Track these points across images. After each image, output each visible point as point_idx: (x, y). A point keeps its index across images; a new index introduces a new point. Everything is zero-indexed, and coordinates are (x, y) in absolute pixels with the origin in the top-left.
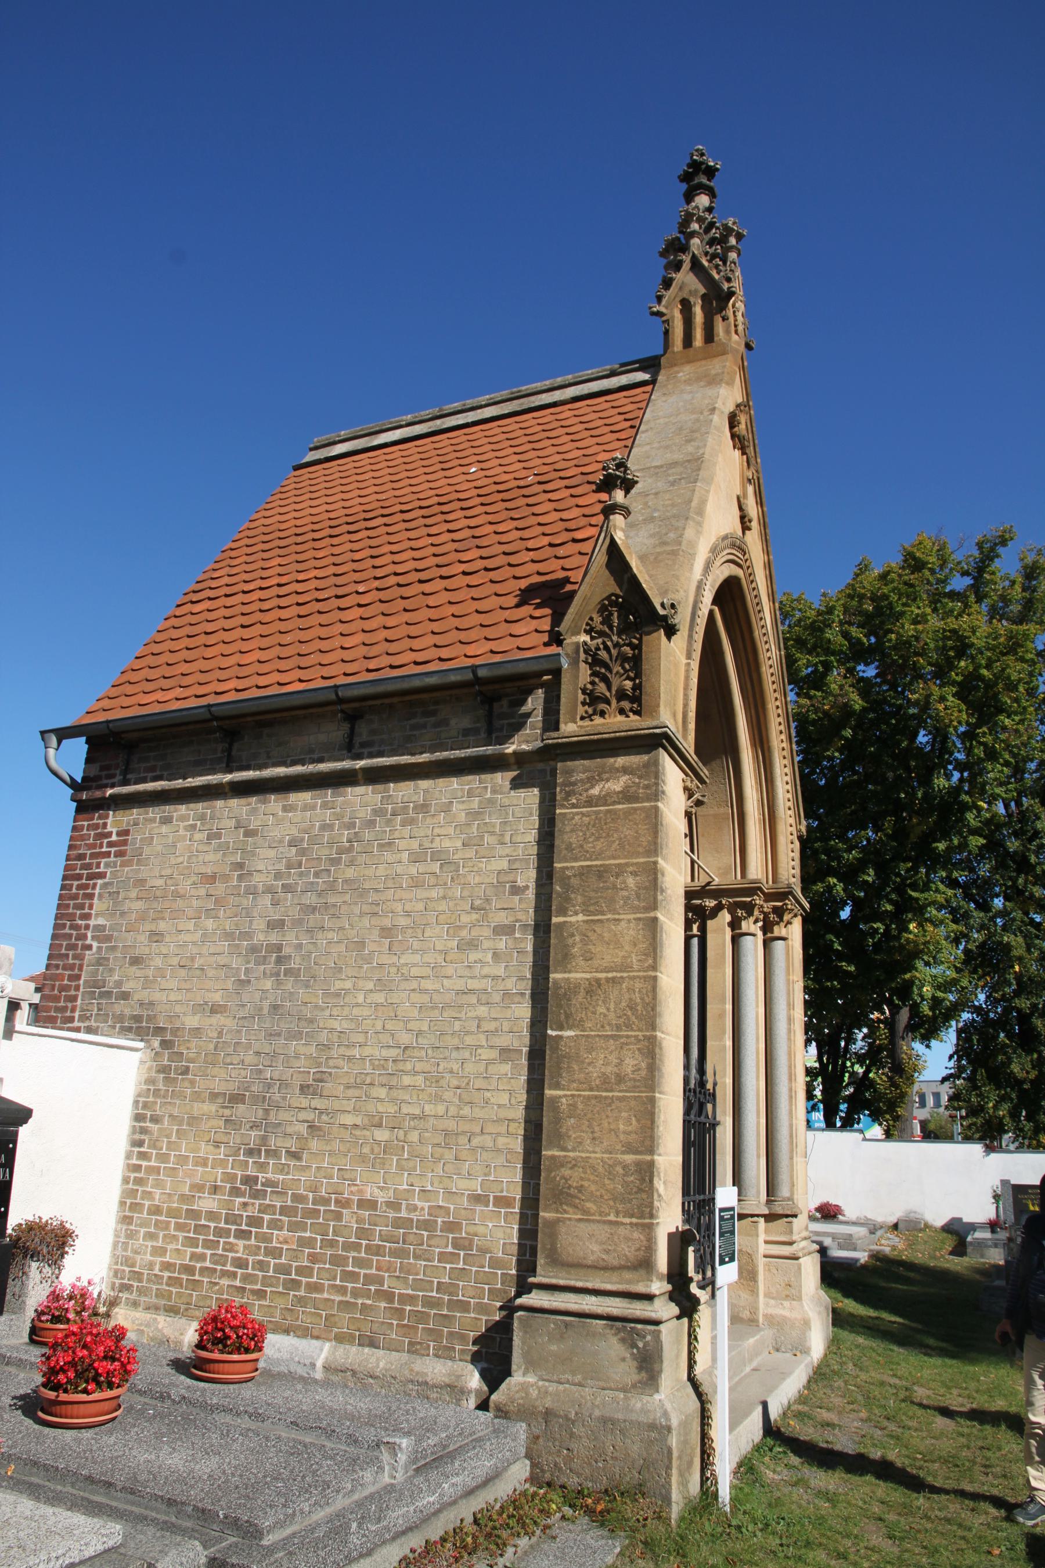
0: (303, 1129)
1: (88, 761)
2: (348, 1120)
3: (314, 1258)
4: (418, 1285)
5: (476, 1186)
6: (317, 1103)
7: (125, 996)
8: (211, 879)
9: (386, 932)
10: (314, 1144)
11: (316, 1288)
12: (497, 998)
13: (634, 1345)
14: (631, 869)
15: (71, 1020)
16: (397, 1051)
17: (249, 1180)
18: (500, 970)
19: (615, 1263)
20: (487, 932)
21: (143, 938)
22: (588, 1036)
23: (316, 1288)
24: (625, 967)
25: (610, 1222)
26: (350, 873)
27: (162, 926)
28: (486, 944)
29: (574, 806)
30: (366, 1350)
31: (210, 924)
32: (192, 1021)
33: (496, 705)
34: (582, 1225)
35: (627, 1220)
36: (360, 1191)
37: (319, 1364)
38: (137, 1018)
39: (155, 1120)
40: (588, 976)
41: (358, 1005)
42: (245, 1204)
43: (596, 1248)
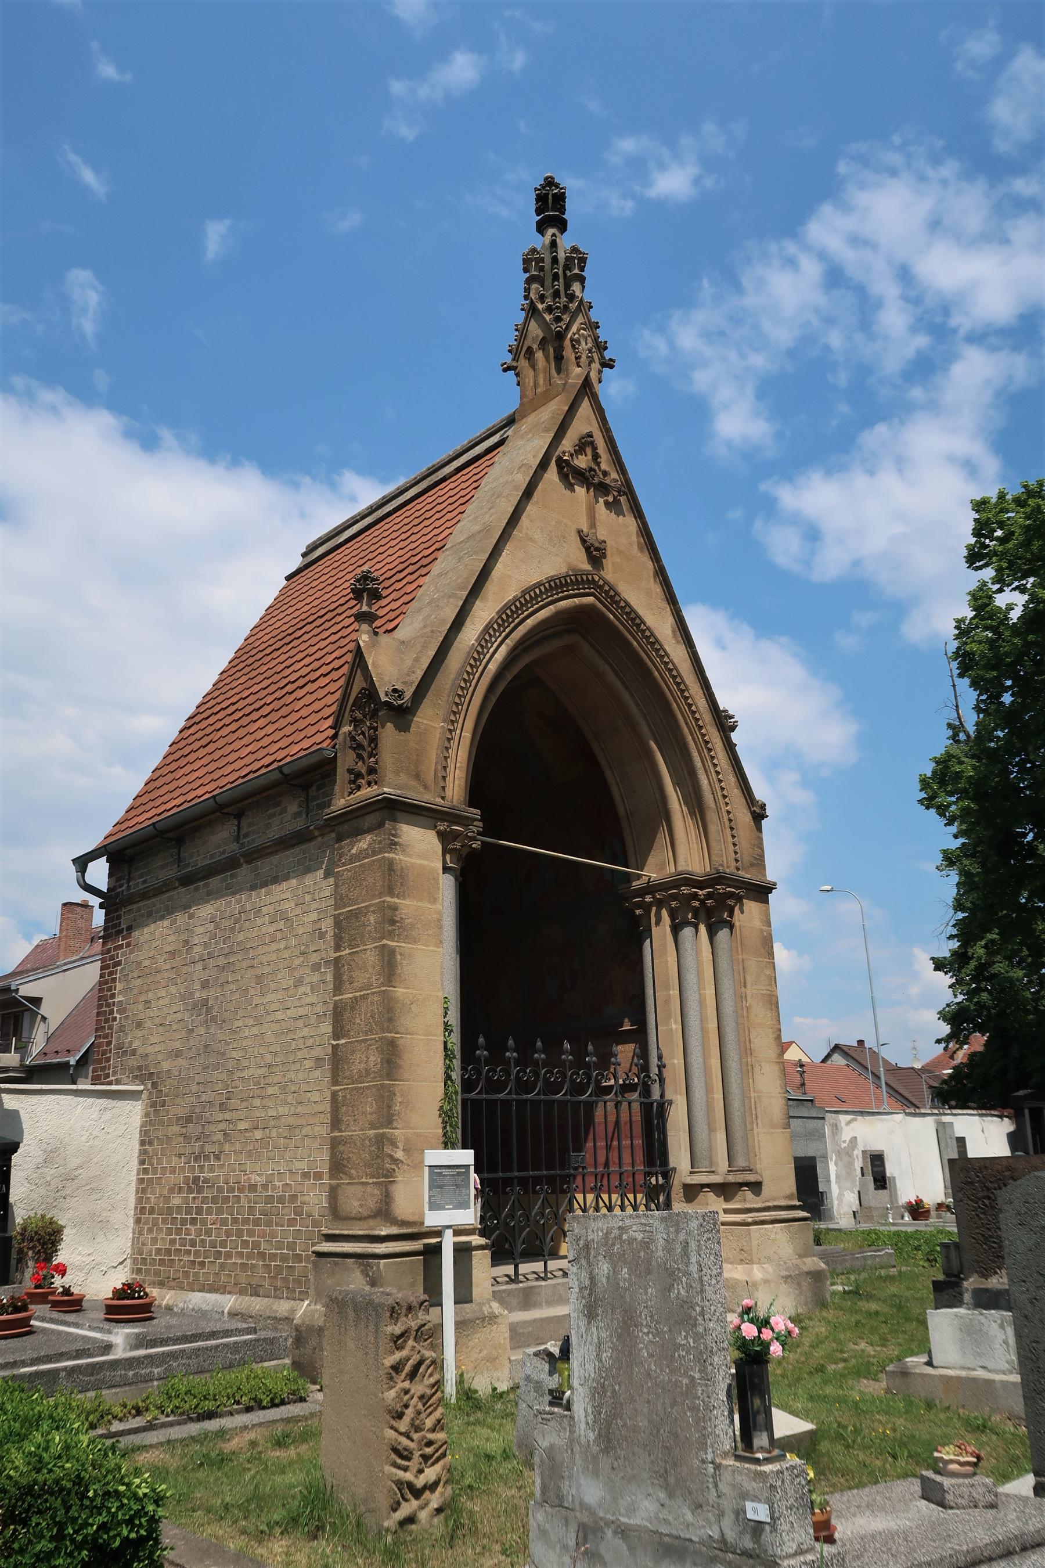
0: (220, 1136)
1: (110, 875)
2: (242, 1126)
3: (228, 1233)
4: (279, 1245)
5: (303, 1166)
6: (228, 1116)
7: (134, 1052)
8: (172, 954)
9: (259, 979)
10: (227, 1147)
11: (228, 1255)
12: (313, 1020)
13: (367, 1275)
14: (372, 909)
15: (107, 1076)
16: (265, 1069)
17: (196, 1179)
18: (313, 999)
19: (365, 1214)
20: (308, 971)
21: (141, 1006)
22: (351, 1042)
23: (228, 1255)
24: (369, 986)
25: (363, 1183)
26: (241, 937)
27: (150, 996)
28: (307, 980)
29: (344, 865)
30: (253, 1298)
31: (173, 989)
32: (166, 1066)
33: (310, 791)
34: (349, 1187)
35: (371, 1181)
36: (249, 1179)
37: (226, 1311)
38: (140, 1068)
39: (151, 1143)
40: (350, 996)
41: (246, 1038)
42: (194, 1198)
43: (356, 1204)
